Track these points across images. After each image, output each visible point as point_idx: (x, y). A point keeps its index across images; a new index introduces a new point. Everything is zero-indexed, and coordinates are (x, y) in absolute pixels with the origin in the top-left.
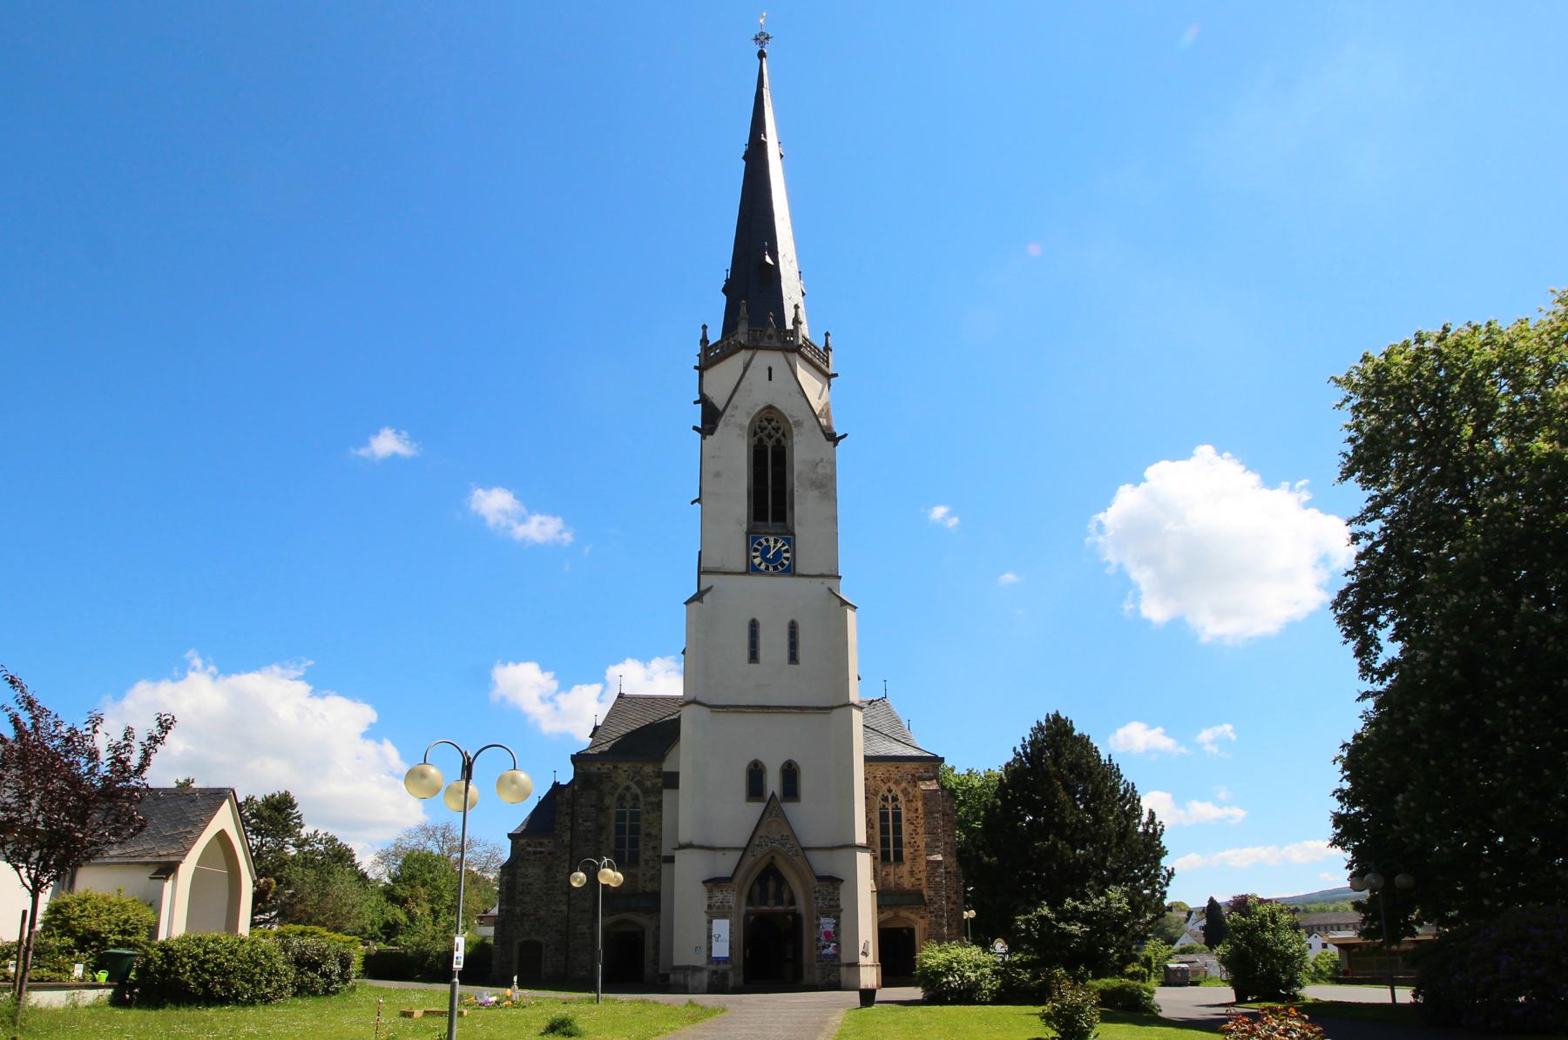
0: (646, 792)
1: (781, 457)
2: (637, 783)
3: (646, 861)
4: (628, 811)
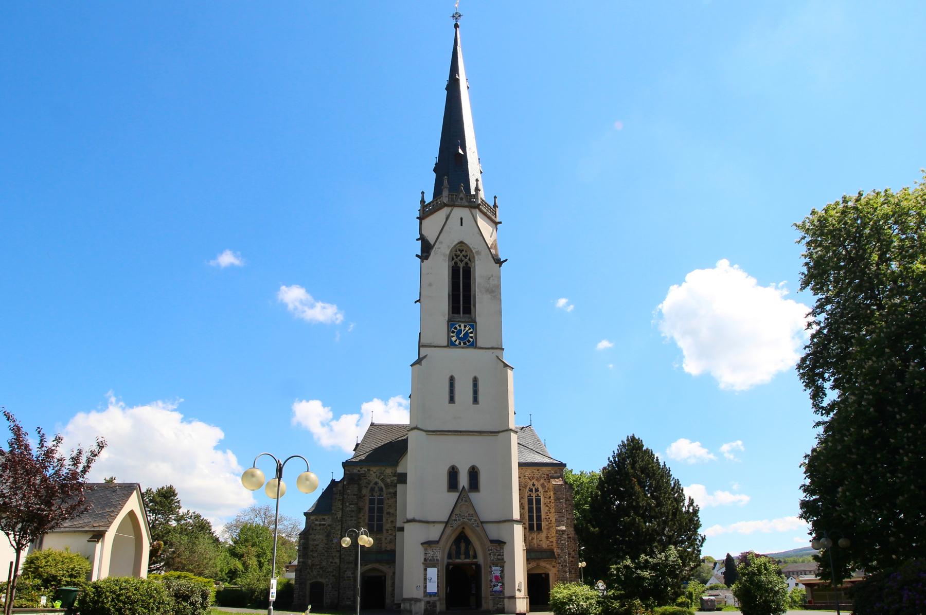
2: (382, 480)
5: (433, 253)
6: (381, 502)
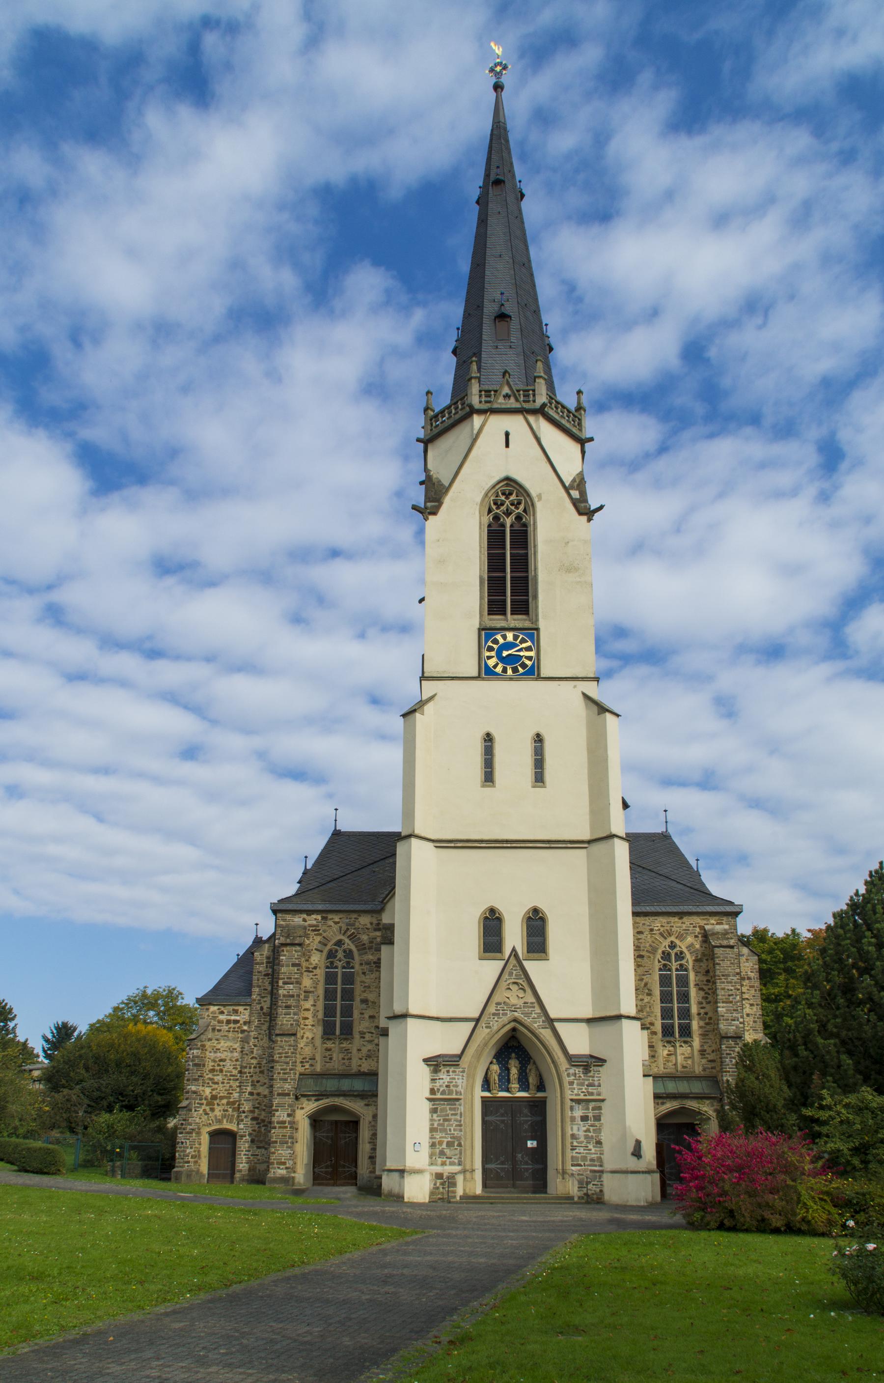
0: (362, 948)
1: (522, 537)
2: (352, 937)
3: (362, 1034)
4: (339, 971)
5: (447, 501)
6: (349, 979)
